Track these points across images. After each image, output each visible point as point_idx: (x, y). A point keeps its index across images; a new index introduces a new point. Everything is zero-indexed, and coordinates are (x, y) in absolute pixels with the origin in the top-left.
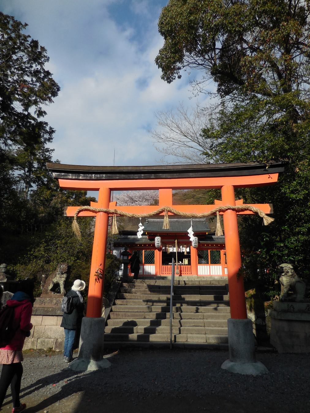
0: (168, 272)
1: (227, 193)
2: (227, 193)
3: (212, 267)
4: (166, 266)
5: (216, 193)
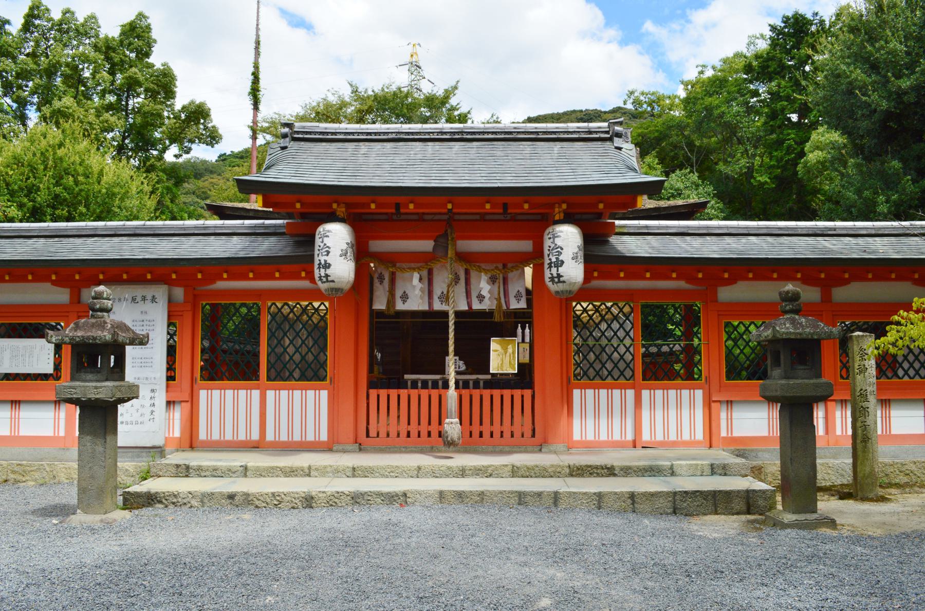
0: (424, 429)
3: (277, 402)
4: (394, 393)
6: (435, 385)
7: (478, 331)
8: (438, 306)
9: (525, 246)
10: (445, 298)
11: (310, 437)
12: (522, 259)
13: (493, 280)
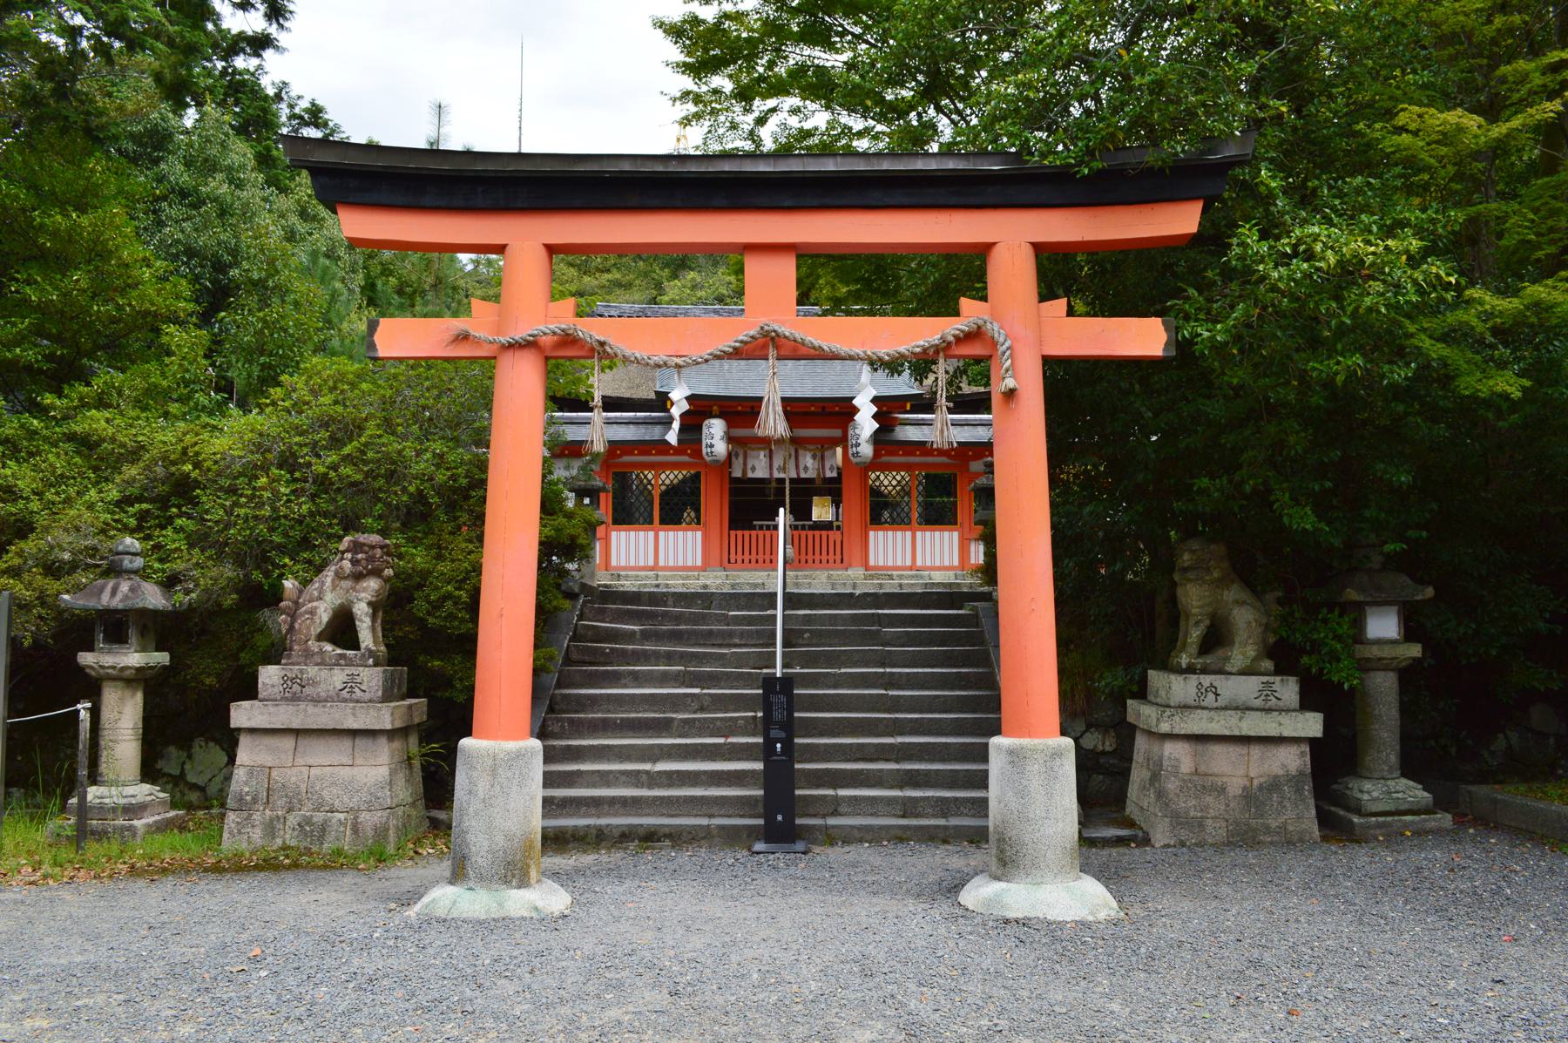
0: (753, 557)
1: (1013, 272)
2: (1013, 272)
3: (666, 539)
4: (747, 533)
5: (960, 275)
6: (768, 527)
7: (802, 495)
8: (777, 475)
9: (837, 433)
10: (783, 469)
11: (690, 563)
12: (835, 442)
13: (814, 457)
